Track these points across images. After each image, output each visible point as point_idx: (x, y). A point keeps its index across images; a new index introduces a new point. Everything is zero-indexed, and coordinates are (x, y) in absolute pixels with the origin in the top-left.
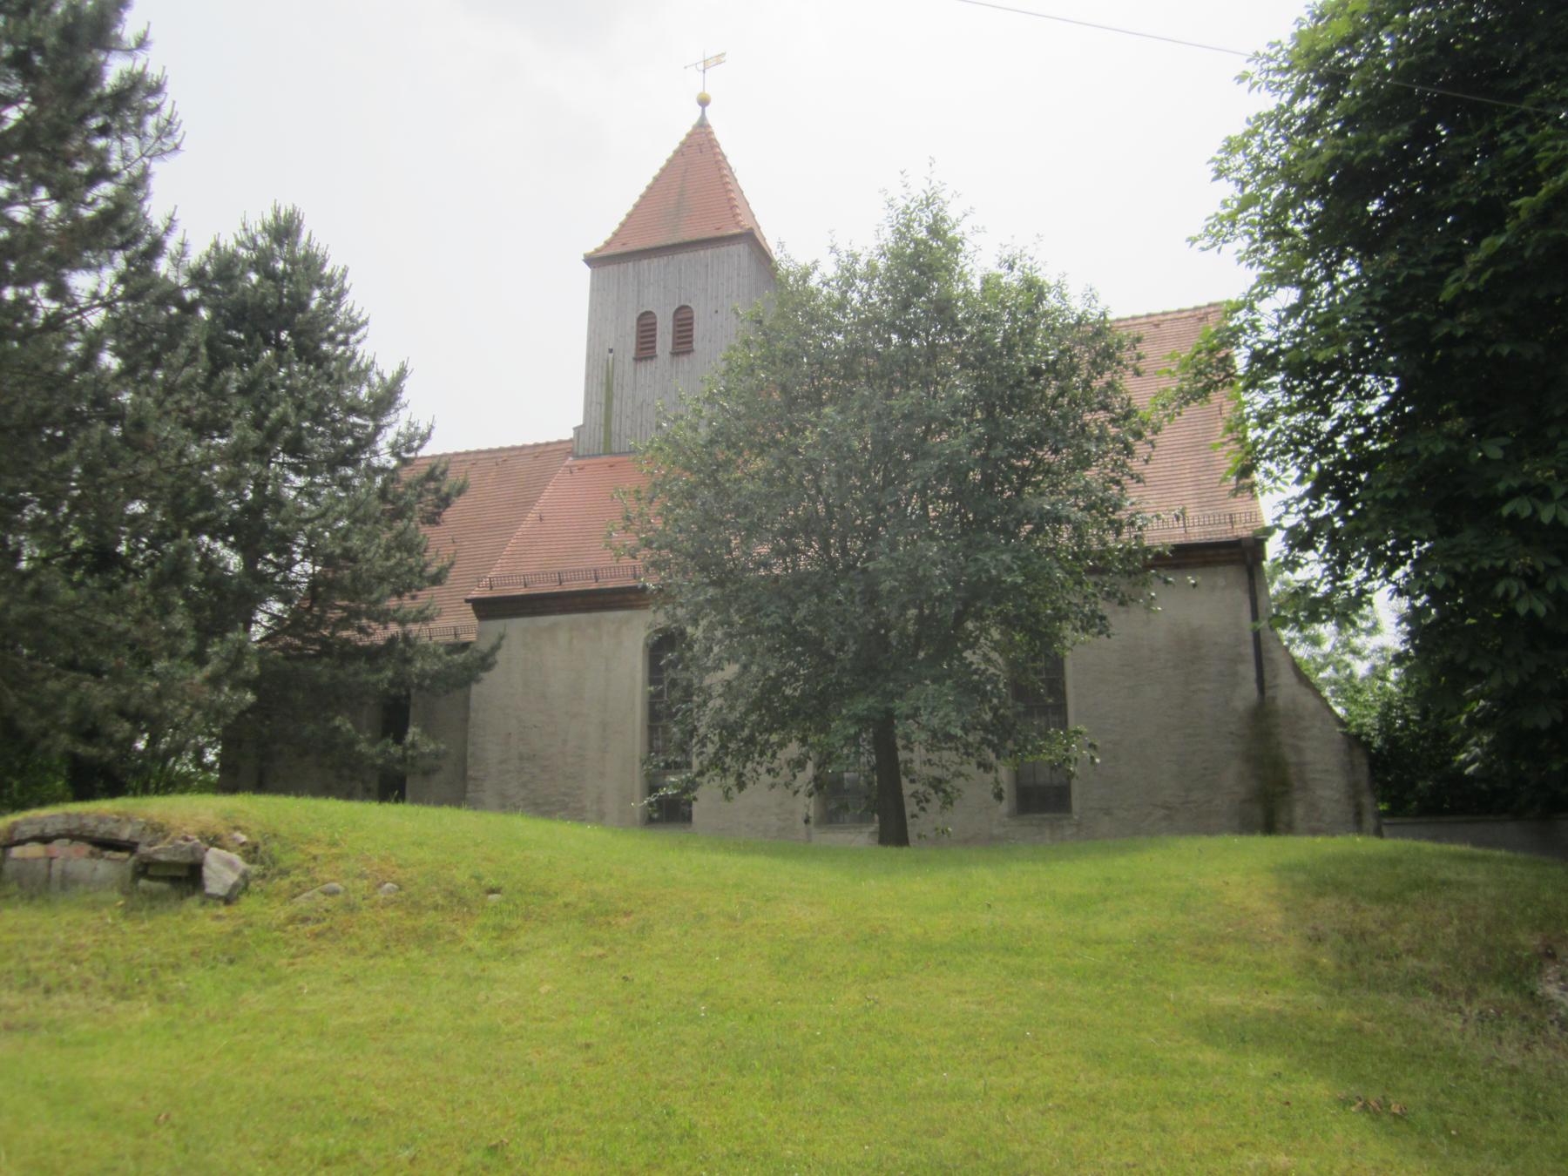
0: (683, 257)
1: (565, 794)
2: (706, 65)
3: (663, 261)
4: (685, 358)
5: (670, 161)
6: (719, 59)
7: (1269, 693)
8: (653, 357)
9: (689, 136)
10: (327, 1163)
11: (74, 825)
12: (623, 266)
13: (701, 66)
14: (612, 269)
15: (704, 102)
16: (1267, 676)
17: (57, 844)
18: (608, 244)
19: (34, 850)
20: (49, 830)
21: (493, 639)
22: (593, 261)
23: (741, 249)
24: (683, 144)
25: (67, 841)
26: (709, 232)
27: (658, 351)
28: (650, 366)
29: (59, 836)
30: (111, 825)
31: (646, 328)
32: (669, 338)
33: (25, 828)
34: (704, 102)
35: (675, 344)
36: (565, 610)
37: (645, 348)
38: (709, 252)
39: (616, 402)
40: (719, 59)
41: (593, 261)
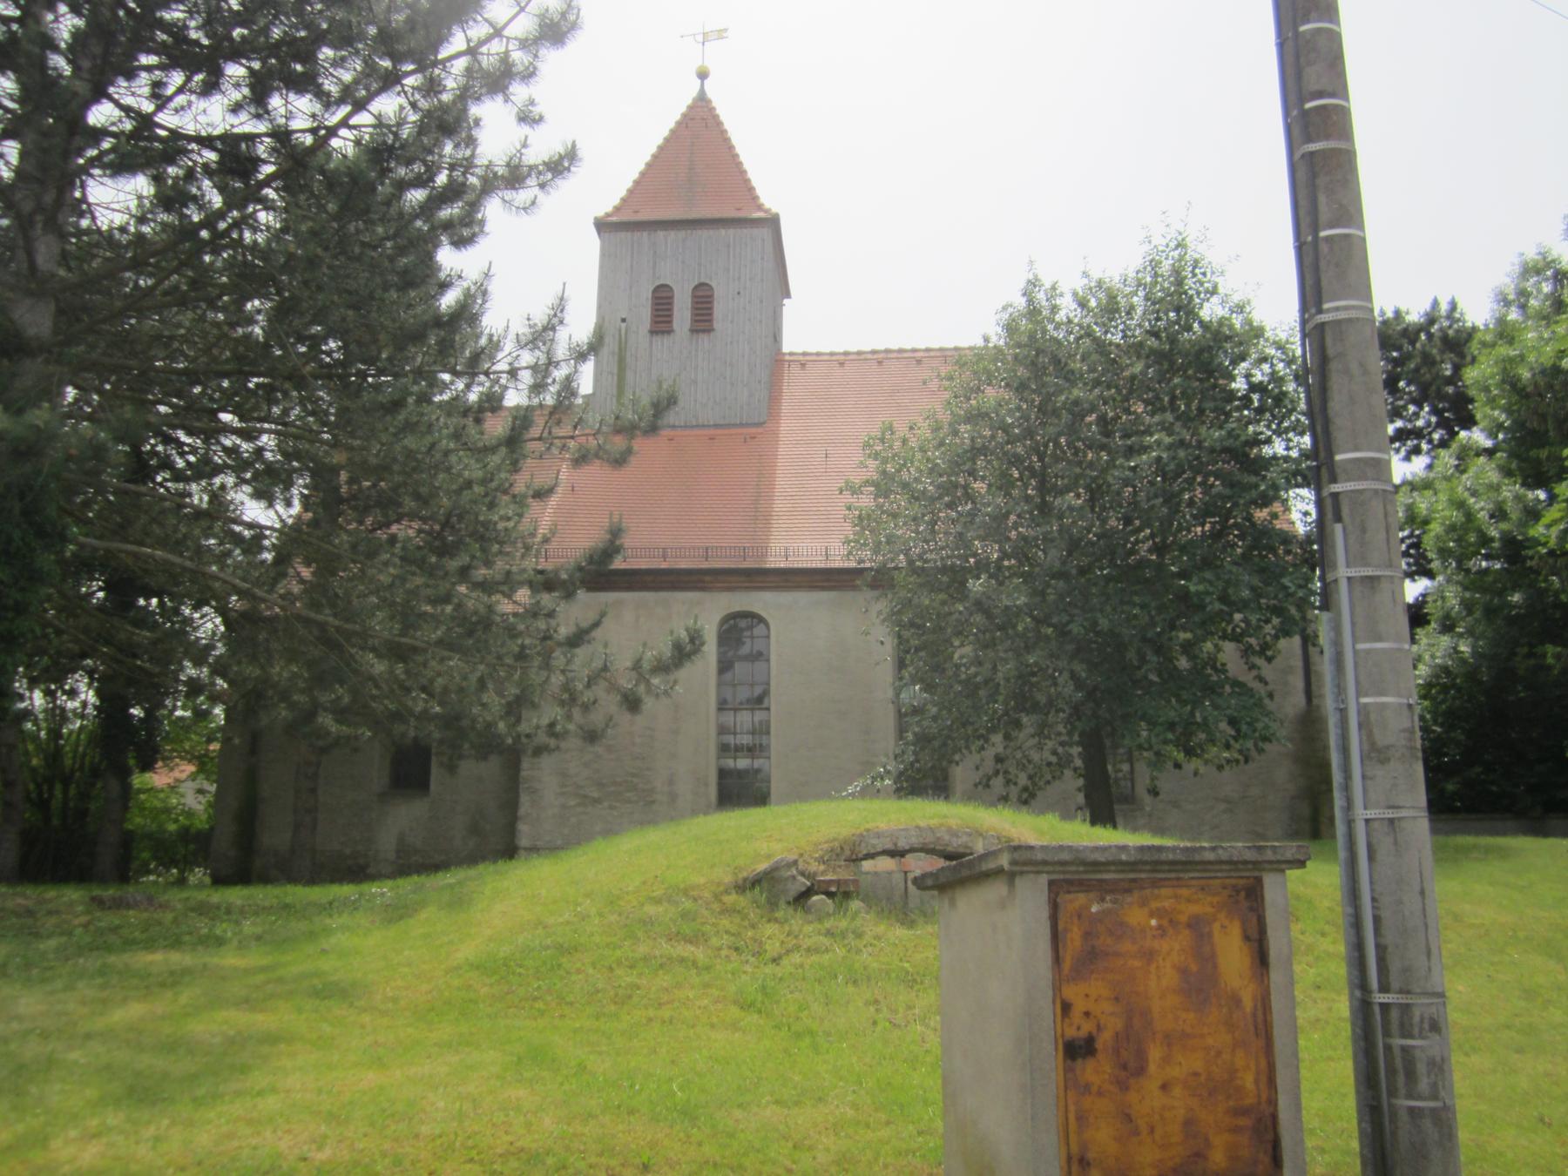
0: (704, 234)
1: (634, 775)
2: (706, 39)
3: (682, 234)
4: (704, 337)
5: (673, 132)
6: (721, 34)
7: (1315, 701)
8: (670, 332)
9: (690, 108)
10: (183, 1169)
11: (929, 838)
12: (637, 235)
13: (700, 38)
14: (624, 236)
15: (703, 75)
16: (1314, 687)
17: (909, 857)
18: (617, 209)
19: (885, 864)
20: (903, 844)
21: (592, 616)
22: (602, 226)
23: (765, 233)
24: (684, 116)
25: (922, 855)
26: (729, 213)
27: (676, 325)
28: (666, 340)
29: (912, 850)
30: (965, 839)
31: (662, 301)
32: (688, 314)
33: (874, 841)
34: (703, 75)
35: (694, 321)
36: (630, 588)
37: (662, 319)
38: (731, 232)
39: (629, 375)
40: (721, 34)
41: (602, 226)
